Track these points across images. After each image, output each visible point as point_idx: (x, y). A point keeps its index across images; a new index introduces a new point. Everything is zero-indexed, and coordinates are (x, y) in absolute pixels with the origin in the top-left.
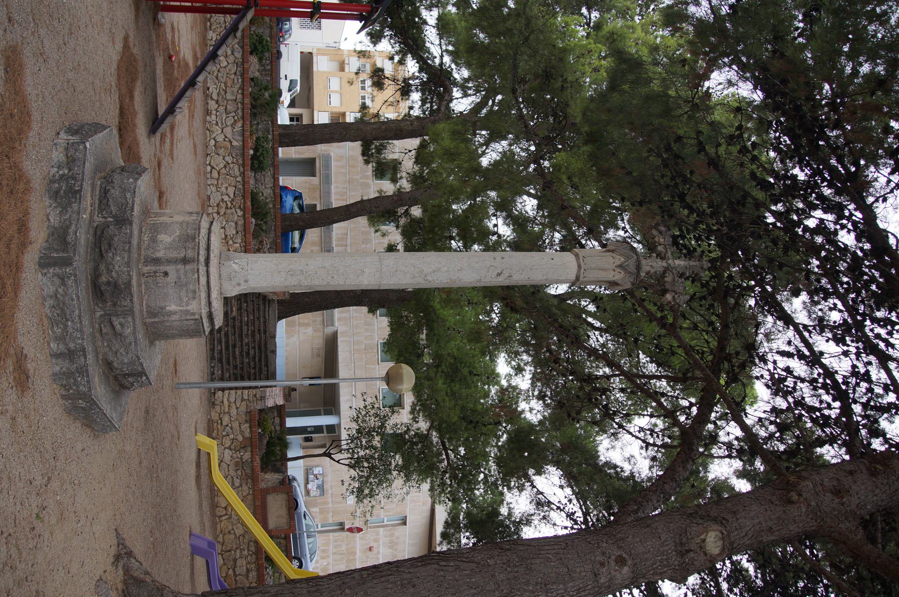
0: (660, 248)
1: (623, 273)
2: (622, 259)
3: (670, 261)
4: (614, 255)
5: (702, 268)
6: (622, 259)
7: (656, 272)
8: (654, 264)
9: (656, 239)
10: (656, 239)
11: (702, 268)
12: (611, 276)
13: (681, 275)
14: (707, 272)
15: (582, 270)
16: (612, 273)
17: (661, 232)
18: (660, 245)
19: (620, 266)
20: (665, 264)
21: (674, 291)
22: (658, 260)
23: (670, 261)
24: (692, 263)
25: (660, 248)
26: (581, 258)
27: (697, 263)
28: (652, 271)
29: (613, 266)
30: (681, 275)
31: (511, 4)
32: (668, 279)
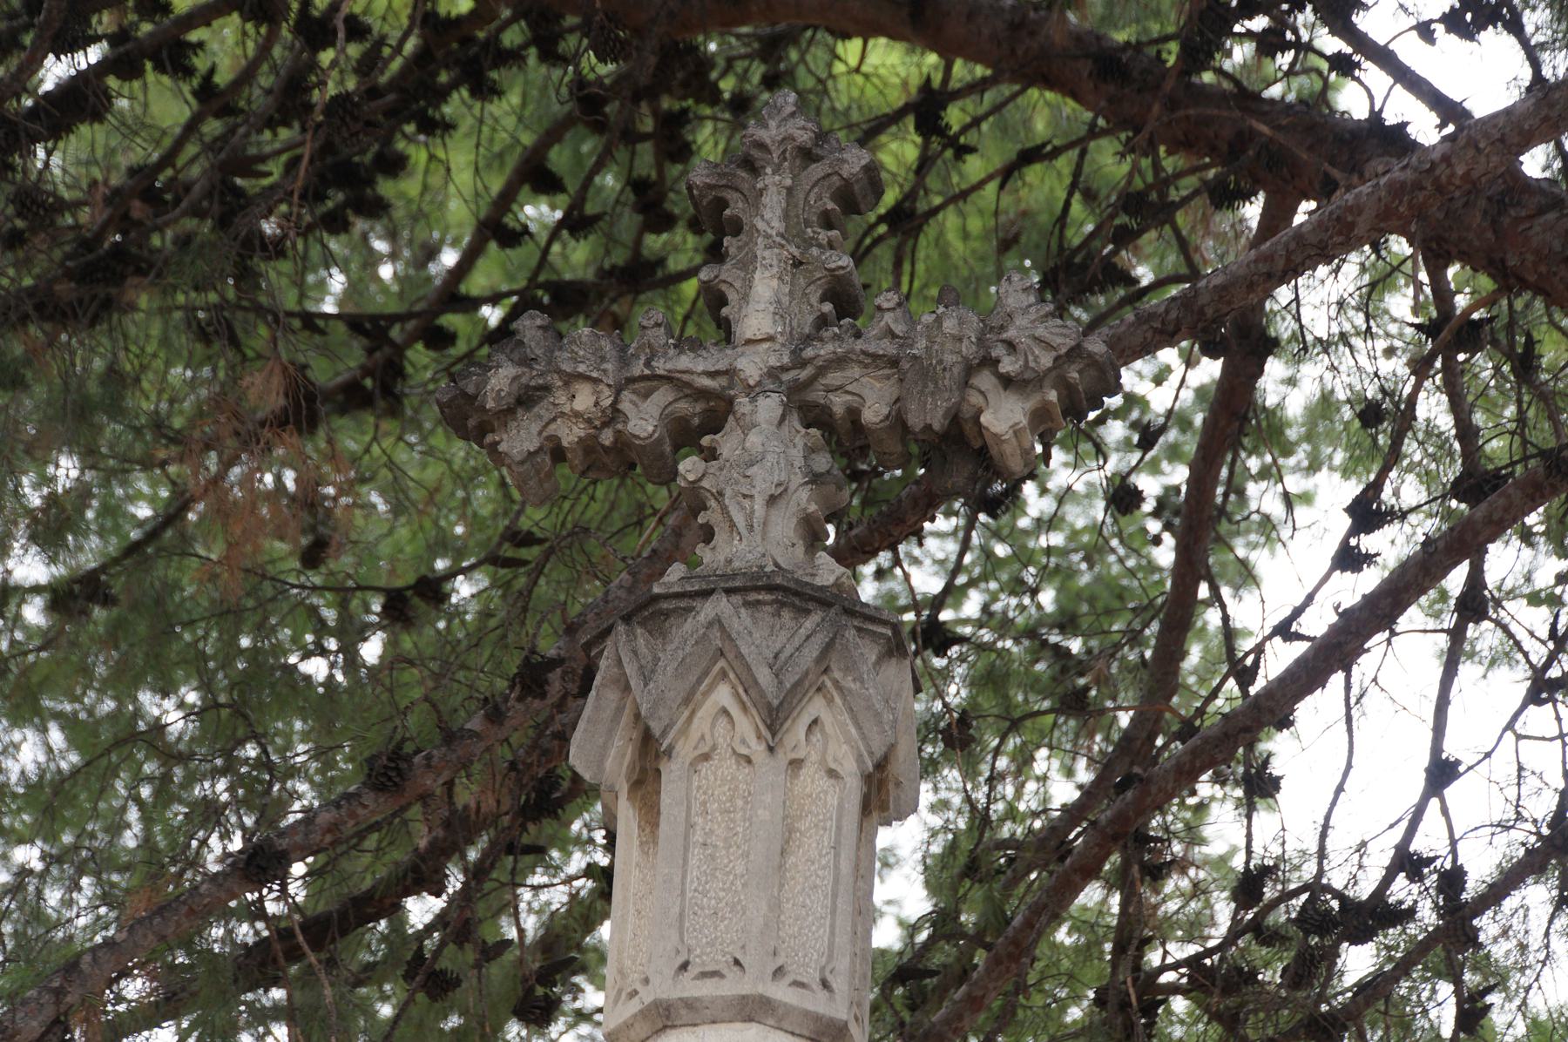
0: (644, 420)
1: (816, 707)
2: (723, 695)
3: (751, 366)
4: (685, 751)
5: (807, 156)
6: (723, 695)
7: (815, 479)
8: (763, 481)
9: (570, 434)
10: (570, 434)
11: (807, 156)
12: (829, 797)
13: (844, 301)
14: (1021, 193)
15: (781, 993)
16: (811, 780)
17: (526, 398)
18: (614, 415)
19: (774, 719)
20: (769, 407)
21: (970, 370)
22: (727, 443)
23: (751, 366)
24: (770, 217)
25: (644, 420)
26: (691, 988)
27: (773, 183)
28: (803, 498)
29: (769, 770)
30: (844, 301)
31: (333, 1040)
32: (875, 402)
